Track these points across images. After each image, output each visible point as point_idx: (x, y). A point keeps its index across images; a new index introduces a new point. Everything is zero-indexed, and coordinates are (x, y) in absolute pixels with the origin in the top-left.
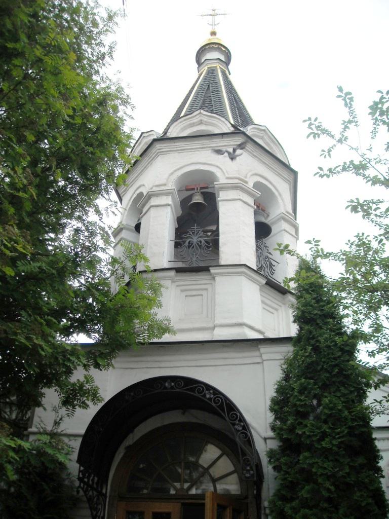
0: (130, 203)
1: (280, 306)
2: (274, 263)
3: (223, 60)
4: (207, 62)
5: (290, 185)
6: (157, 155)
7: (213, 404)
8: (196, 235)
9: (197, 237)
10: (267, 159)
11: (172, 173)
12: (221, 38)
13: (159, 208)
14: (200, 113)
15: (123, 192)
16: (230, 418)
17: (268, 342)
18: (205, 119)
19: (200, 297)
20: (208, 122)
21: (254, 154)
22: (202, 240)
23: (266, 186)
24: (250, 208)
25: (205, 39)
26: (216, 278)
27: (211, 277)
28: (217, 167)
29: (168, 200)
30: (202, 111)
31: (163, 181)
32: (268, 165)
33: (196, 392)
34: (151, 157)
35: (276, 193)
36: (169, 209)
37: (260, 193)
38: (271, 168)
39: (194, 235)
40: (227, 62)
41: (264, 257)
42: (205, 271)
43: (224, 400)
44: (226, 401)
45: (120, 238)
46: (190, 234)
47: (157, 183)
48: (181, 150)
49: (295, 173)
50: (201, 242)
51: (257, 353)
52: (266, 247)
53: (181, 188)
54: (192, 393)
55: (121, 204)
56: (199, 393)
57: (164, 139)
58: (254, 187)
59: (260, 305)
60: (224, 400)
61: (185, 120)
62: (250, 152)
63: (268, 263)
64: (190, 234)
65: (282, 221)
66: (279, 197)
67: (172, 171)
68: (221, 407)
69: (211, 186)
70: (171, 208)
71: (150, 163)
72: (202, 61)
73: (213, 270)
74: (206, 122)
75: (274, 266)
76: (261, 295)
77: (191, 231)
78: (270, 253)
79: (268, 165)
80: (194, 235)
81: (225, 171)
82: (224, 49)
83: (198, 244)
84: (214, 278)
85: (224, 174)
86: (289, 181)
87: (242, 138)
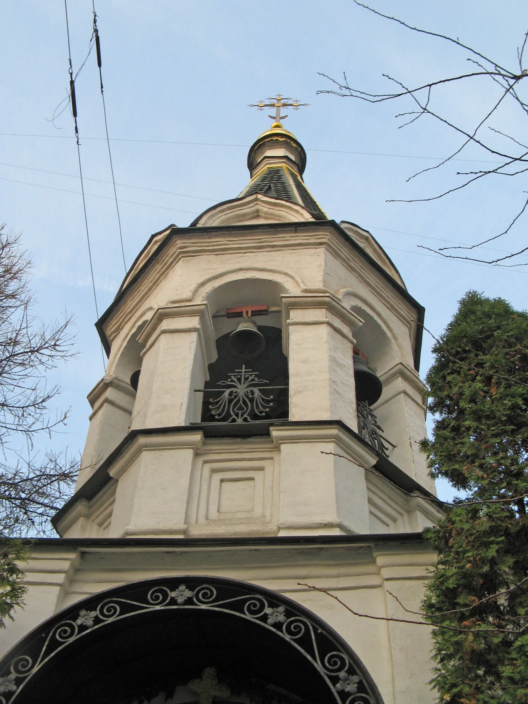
0: (125, 344)
1: (401, 515)
2: (386, 445)
3: (293, 158)
4: (266, 161)
5: (410, 329)
6: (176, 260)
7: (287, 638)
8: (244, 383)
9: (246, 385)
10: (373, 278)
11: (203, 284)
12: (289, 127)
13: (176, 335)
14: (256, 199)
15: (112, 333)
16: (327, 664)
17: (391, 543)
18: (265, 209)
19: (250, 483)
20: (271, 214)
21: (351, 264)
22: (256, 390)
23: (372, 317)
24: (345, 341)
25: (266, 128)
26: (283, 447)
27: (271, 446)
28: (286, 274)
29: (194, 322)
30: (260, 196)
31: (187, 294)
32: (373, 288)
33: (246, 612)
34: (166, 263)
35: (389, 334)
36: (194, 336)
37: (363, 321)
38: (381, 296)
39: (240, 383)
40: (301, 164)
41: (370, 430)
42: (262, 435)
43: (311, 628)
44: (315, 630)
45: (103, 399)
46: (232, 381)
47: (175, 298)
48: (221, 250)
49: (420, 311)
50: (252, 393)
51: (371, 568)
52: (372, 416)
53: (217, 312)
54: (238, 614)
55: (108, 358)
56: (251, 612)
57: (193, 230)
58: (350, 309)
59: (366, 507)
60: (311, 628)
61: (229, 208)
62: (344, 261)
63: (376, 441)
64: (232, 381)
65: (400, 378)
66: (393, 341)
67: (201, 280)
68: (305, 642)
69: (273, 309)
70: (199, 335)
71: (164, 274)
72: (259, 161)
73: (275, 433)
74: (266, 213)
75: (387, 449)
76: (367, 488)
77: (235, 376)
78: (379, 428)
79: (373, 288)
80: (240, 383)
81: (299, 281)
82: (294, 145)
83: (247, 396)
84: (277, 449)
85: (298, 284)
86: (408, 322)
87: (330, 232)
